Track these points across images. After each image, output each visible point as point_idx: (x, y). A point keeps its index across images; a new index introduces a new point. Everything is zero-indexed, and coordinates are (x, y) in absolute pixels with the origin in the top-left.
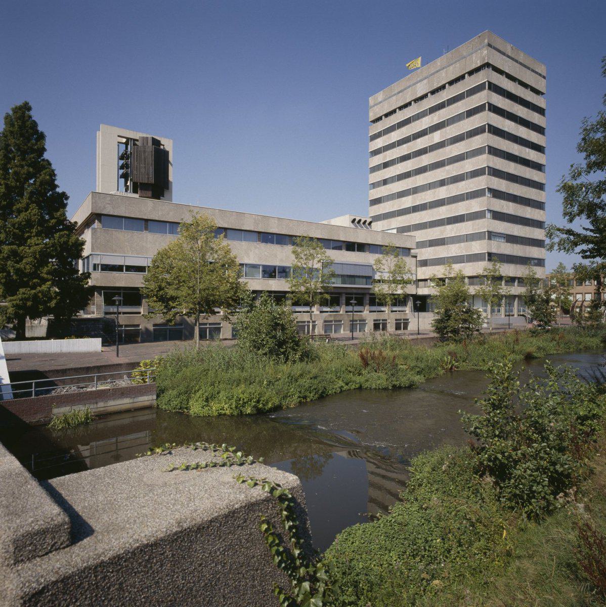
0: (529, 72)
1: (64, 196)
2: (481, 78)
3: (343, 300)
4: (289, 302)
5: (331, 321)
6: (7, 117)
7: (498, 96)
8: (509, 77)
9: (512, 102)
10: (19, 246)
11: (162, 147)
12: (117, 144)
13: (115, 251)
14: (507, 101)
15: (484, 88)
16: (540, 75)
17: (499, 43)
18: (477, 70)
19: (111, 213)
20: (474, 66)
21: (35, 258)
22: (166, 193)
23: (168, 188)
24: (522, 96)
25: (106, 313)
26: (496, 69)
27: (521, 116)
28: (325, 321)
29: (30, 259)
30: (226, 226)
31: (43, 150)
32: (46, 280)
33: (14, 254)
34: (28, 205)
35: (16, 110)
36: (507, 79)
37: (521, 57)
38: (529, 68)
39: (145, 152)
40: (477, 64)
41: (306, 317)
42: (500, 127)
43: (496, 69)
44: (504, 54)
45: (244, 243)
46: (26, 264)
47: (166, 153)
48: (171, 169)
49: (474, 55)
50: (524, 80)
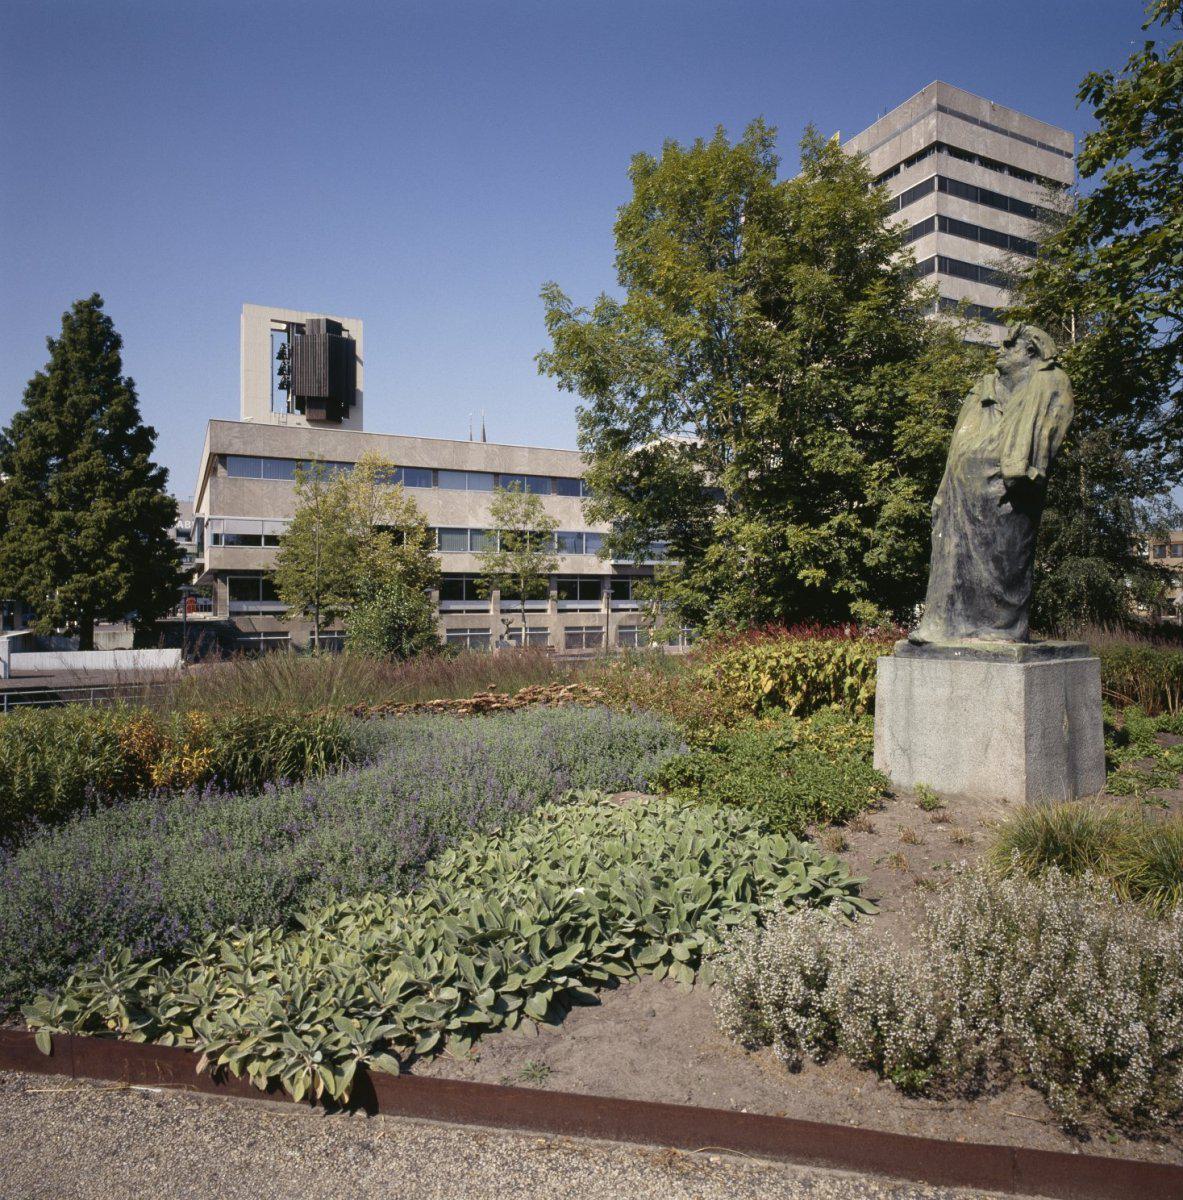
0: (1032, 150)
1: (150, 432)
2: (926, 171)
3: (606, 592)
4: (496, 594)
5: (633, 627)
6: (67, 318)
7: (961, 200)
8: (988, 163)
9: (994, 210)
10: (76, 510)
11: (344, 335)
12: (269, 332)
13: (248, 514)
14: (982, 209)
15: (932, 189)
16: (1060, 152)
17: (962, 101)
18: (921, 155)
19: (241, 452)
20: (914, 149)
21: (100, 529)
22: (352, 412)
23: (354, 404)
24: (1018, 196)
25: (232, 613)
26: (957, 153)
27: (1016, 234)
28: (620, 627)
29: (92, 531)
30: (435, 465)
31: (117, 365)
32: (113, 560)
33: (69, 523)
34: (90, 451)
35: (80, 308)
36: (981, 168)
37: (1015, 123)
38: (1032, 142)
39: (314, 345)
40: (918, 144)
41: (475, 622)
42: (967, 259)
43: (957, 153)
44: (975, 121)
45: (467, 493)
46: (85, 540)
47: (350, 344)
48: (360, 370)
49: (914, 128)
50: (1022, 166)
